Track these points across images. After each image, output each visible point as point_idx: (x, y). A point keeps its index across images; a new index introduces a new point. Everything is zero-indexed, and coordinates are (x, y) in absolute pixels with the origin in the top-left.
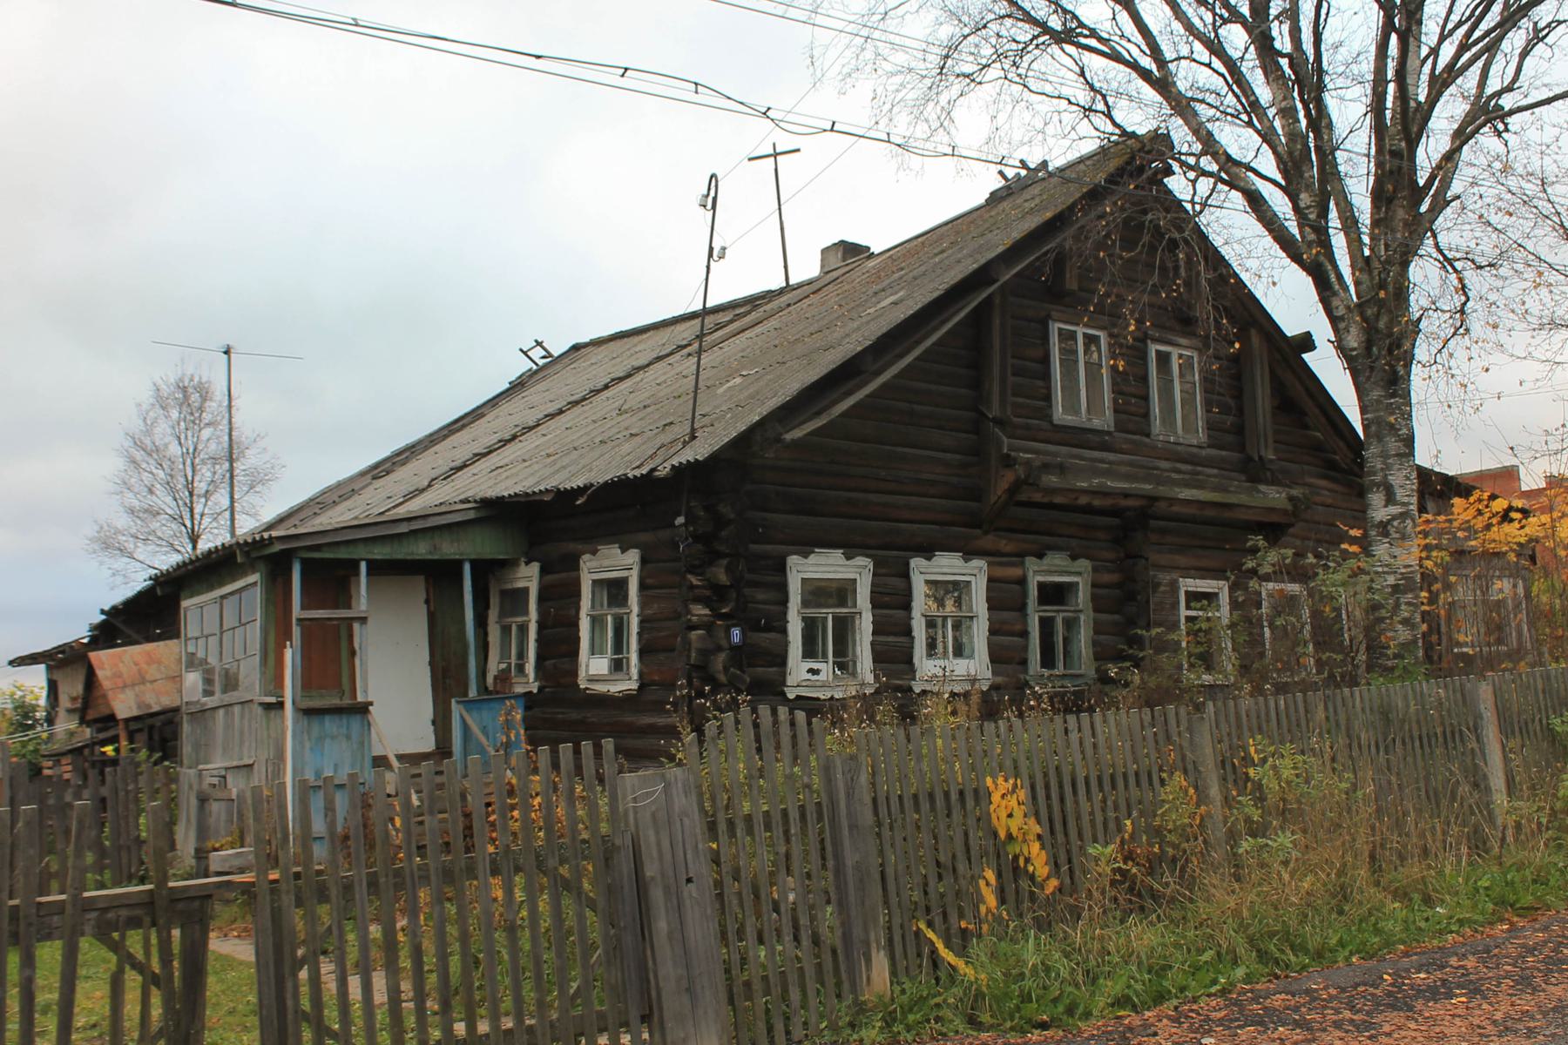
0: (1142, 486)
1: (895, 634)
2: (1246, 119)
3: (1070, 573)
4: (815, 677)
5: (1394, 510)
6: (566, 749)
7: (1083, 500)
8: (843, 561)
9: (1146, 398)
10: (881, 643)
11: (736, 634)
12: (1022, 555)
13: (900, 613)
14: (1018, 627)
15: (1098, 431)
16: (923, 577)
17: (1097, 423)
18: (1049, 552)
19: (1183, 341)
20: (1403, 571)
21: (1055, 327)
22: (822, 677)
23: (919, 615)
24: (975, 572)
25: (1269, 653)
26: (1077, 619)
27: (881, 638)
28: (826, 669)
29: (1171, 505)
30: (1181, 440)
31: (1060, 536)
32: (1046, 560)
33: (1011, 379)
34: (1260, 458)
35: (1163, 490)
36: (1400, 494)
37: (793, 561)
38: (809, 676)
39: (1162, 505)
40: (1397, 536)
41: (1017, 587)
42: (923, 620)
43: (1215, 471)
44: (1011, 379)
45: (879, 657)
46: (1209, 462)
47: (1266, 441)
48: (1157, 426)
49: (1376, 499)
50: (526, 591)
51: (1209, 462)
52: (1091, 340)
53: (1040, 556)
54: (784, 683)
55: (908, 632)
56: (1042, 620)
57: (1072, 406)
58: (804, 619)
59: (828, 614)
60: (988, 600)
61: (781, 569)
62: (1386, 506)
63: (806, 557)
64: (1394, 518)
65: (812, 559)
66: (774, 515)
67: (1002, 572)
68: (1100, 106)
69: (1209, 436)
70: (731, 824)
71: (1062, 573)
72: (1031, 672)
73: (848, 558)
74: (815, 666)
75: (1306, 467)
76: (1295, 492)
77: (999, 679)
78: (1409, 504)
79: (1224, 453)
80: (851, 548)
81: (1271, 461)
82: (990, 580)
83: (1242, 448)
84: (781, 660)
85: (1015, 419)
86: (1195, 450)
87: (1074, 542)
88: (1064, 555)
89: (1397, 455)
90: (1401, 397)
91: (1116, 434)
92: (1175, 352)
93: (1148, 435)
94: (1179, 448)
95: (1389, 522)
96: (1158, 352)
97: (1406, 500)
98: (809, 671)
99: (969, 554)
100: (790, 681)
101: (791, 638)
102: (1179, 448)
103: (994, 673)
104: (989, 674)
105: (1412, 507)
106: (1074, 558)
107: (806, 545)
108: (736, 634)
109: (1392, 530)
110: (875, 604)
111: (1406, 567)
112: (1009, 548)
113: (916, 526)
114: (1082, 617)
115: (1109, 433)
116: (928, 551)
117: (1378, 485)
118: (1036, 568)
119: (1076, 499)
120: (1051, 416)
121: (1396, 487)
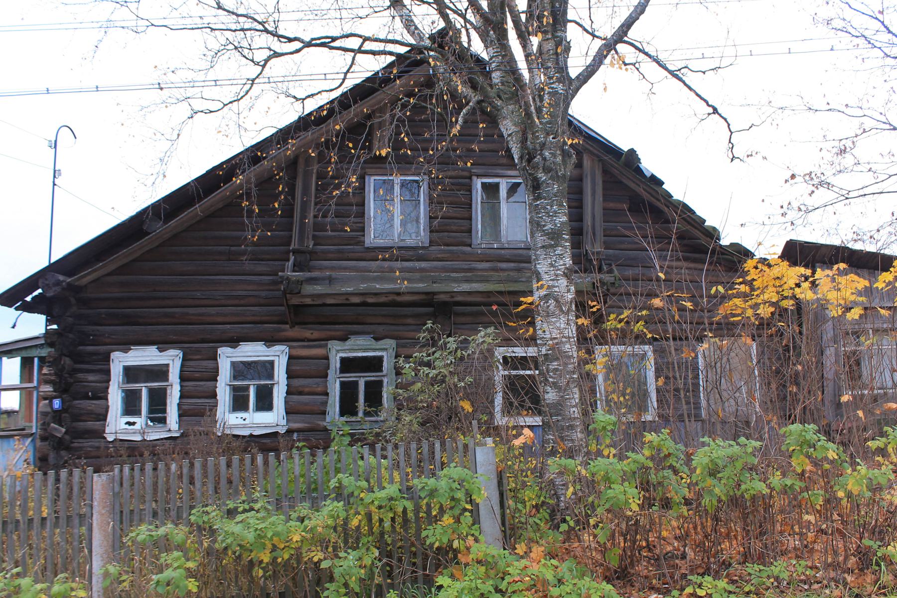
0: (415, 285)
3: (375, 350)
4: (132, 427)
6: (64, 473)
8: (157, 353)
15: (412, 248)
16: (229, 360)
18: (352, 337)
22: (137, 427)
23: (223, 385)
24: (277, 354)
28: (140, 421)
32: (348, 343)
35: (436, 287)
38: (127, 426)
54: (104, 432)
56: (343, 384)
58: (123, 391)
59: (362, 380)
61: (107, 359)
63: (126, 353)
65: (131, 353)
66: (103, 327)
67: (297, 352)
68: (246, 52)
70: (69, 518)
71: (365, 350)
74: (132, 420)
80: (163, 344)
82: (291, 358)
89: (543, 247)
98: (127, 423)
99: (270, 341)
100: (107, 430)
103: (288, 421)
104: (284, 422)
107: (126, 345)
110: (183, 378)
112: (316, 335)
113: (228, 326)
114: (385, 380)
115: (423, 248)
116: (234, 341)
121: (542, 274)
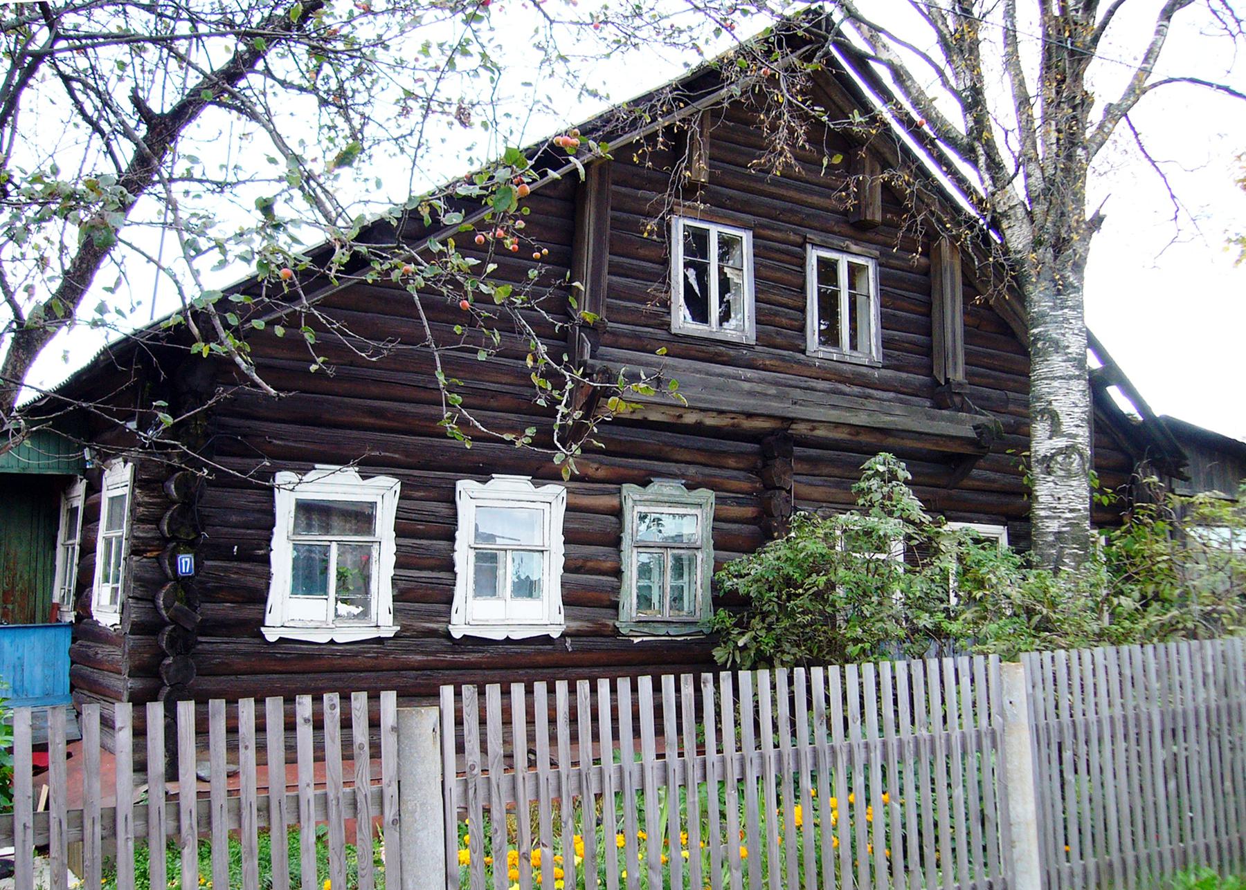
1: (432, 569)
2: (932, 9)
5: (1061, 443)
7: (690, 418)
9: (803, 310)
10: (409, 579)
11: (186, 563)
12: (621, 481)
13: (442, 544)
14: (608, 565)
17: (860, 357)
19: (854, 248)
20: (1069, 515)
21: (813, 255)
23: (465, 547)
25: (686, 609)
26: (692, 560)
27: (402, 572)
29: (813, 429)
30: (848, 359)
31: (677, 462)
32: (652, 489)
33: (606, 279)
34: (947, 380)
36: (1067, 425)
37: (283, 477)
39: (801, 428)
40: (1062, 473)
41: (613, 519)
42: (472, 553)
43: (892, 395)
44: (606, 279)
45: (402, 595)
46: (883, 386)
47: (955, 364)
48: (813, 340)
49: (1040, 429)
50: (77, 508)
51: (883, 386)
52: (727, 245)
53: (644, 483)
54: (262, 623)
55: (450, 567)
57: (830, 336)
58: (296, 548)
60: (566, 532)
62: (1050, 438)
64: (1060, 451)
69: (885, 356)
72: (624, 615)
73: (364, 478)
75: (1011, 395)
76: (980, 419)
77: (575, 625)
78: (1075, 436)
79: (904, 375)
81: (960, 385)
82: (570, 509)
83: (929, 371)
84: (260, 597)
85: (610, 324)
86: (864, 370)
87: (692, 470)
88: (677, 483)
90: (1072, 308)
91: (758, 348)
92: (843, 261)
93: (803, 352)
94: (845, 367)
95: (1053, 455)
96: (820, 260)
97: (1074, 431)
101: (274, 569)
102: (845, 367)
104: (561, 618)
105: (1080, 440)
106: (691, 487)
108: (186, 563)
109: (1056, 467)
110: (400, 532)
111: (1071, 511)
112: (601, 473)
114: (700, 555)
117: (1042, 412)
118: (637, 497)
119: (680, 416)
120: (669, 325)
